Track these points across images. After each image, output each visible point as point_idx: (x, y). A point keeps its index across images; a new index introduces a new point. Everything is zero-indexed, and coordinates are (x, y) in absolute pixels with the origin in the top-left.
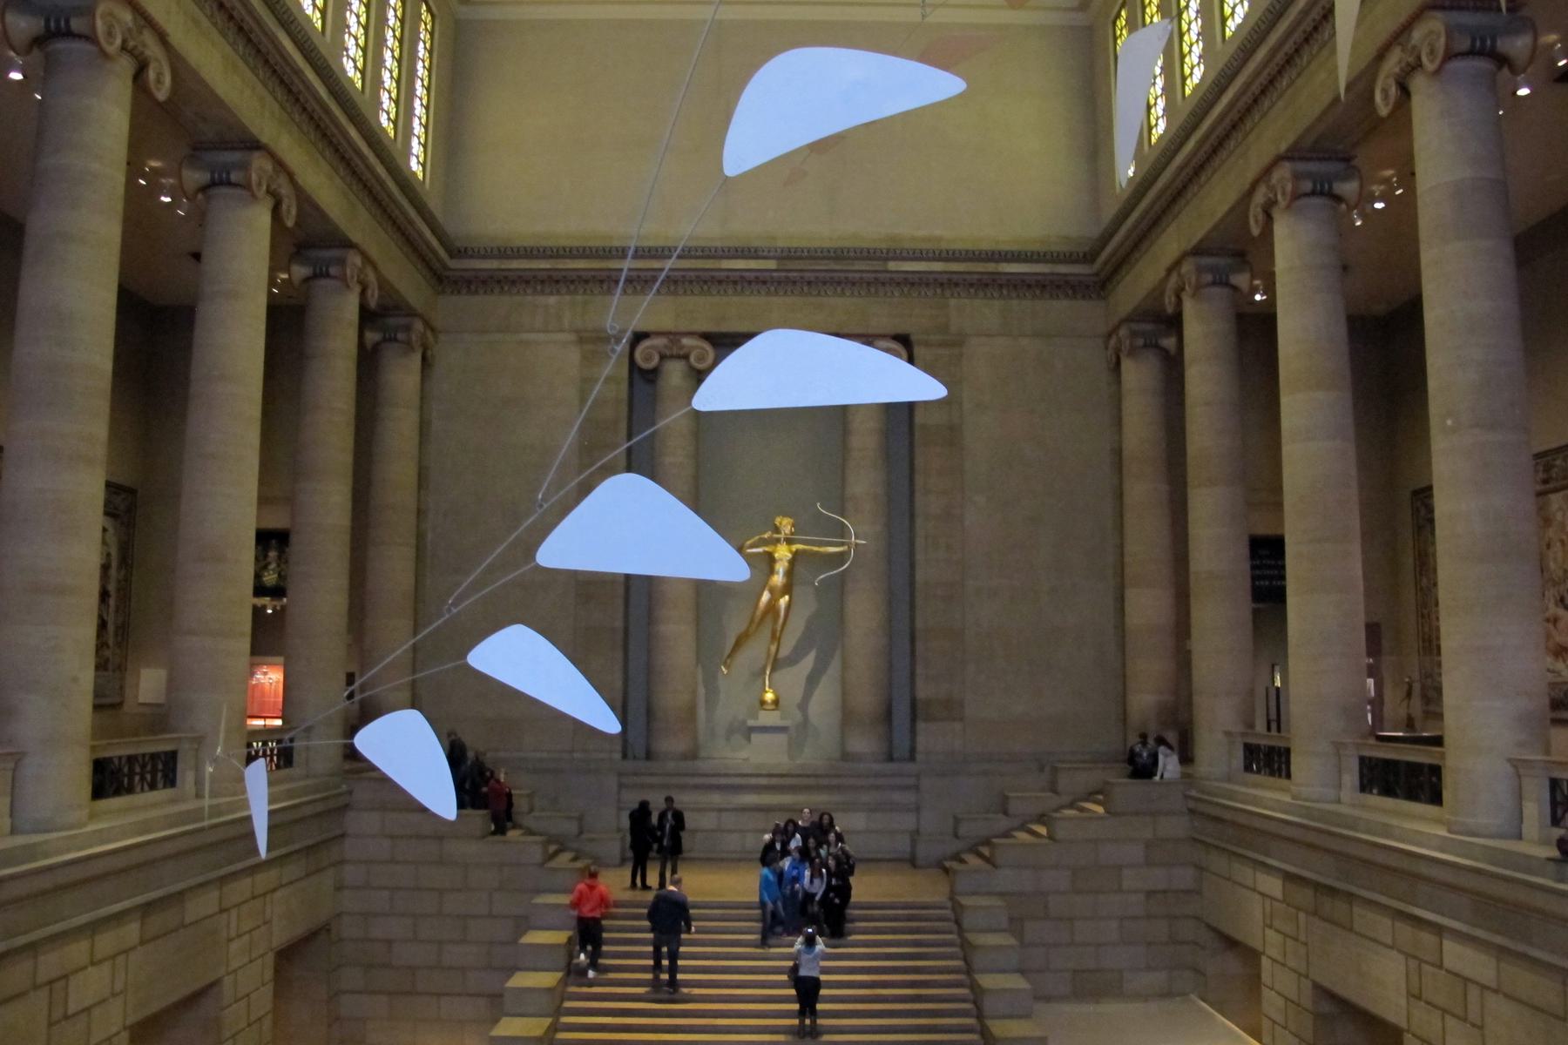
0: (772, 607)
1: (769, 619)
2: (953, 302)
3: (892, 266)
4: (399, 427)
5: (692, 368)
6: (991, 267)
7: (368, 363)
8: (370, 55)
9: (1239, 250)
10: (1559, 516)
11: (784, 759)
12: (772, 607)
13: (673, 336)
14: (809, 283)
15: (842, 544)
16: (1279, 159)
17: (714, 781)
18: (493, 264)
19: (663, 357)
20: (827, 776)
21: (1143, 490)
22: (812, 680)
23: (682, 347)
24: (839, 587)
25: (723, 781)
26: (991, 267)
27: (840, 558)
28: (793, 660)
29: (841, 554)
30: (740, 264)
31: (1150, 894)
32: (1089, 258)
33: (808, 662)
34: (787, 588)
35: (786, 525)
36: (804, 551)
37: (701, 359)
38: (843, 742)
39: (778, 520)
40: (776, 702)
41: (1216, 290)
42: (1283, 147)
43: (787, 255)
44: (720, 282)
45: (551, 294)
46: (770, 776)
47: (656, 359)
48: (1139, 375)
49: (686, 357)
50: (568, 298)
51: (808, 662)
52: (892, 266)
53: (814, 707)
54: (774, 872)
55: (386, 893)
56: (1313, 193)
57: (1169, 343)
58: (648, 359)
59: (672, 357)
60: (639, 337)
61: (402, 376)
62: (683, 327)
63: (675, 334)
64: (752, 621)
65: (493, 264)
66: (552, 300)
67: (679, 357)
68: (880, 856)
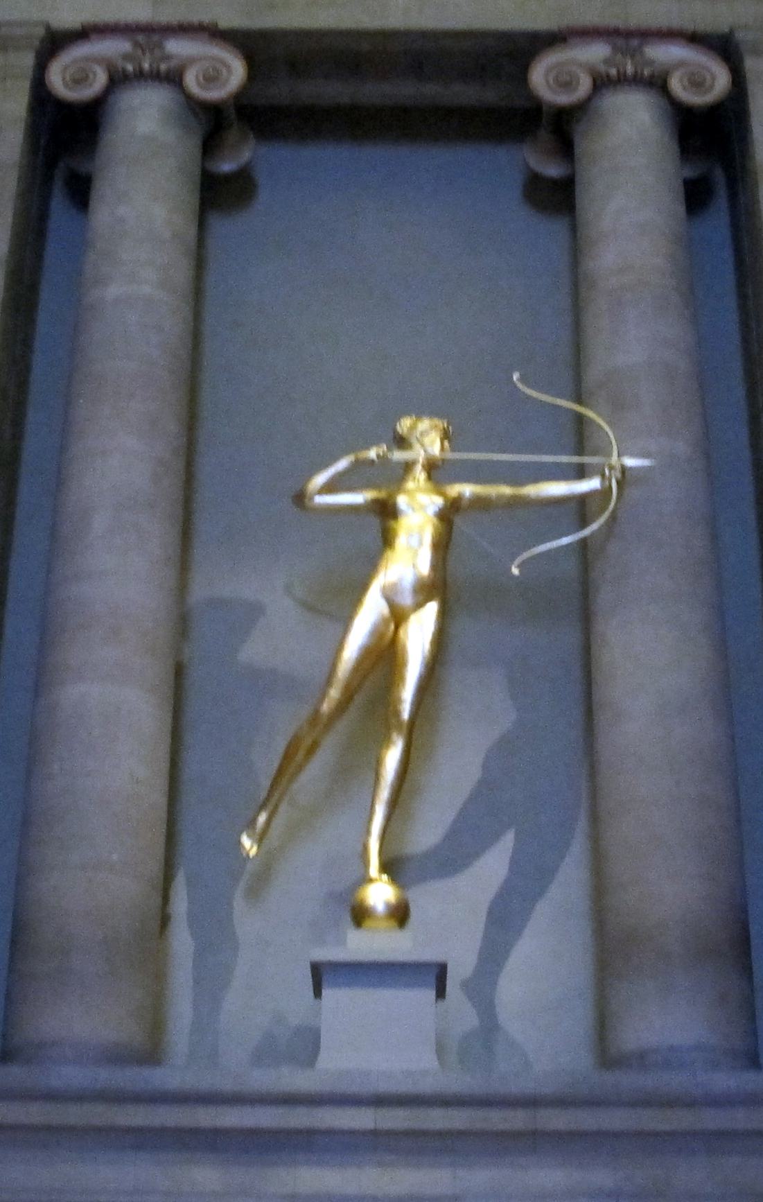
0: (384, 654)
5: (189, 99)
11: (427, 1060)
12: (384, 654)
15: (581, 473)
17: (206, 1117)
20: (561, 1102)
22: (505, 919)
23: (168, 58)
24: (576, 595)
25: (231, 1118)
27: (582, 508)
28: (452, 857)
29: (582, 500)
33: (493, 866)
35: (428, 439)
36: (480, 503)
38: (603, 1025)
39: (405, 425)
46: (380, 1101)
47: (100, 80)
51: (493, 866)
53: (516, 988)
58: (80, 80)
59: (140, 76)
62: (167, 16)
67: (637, 81)
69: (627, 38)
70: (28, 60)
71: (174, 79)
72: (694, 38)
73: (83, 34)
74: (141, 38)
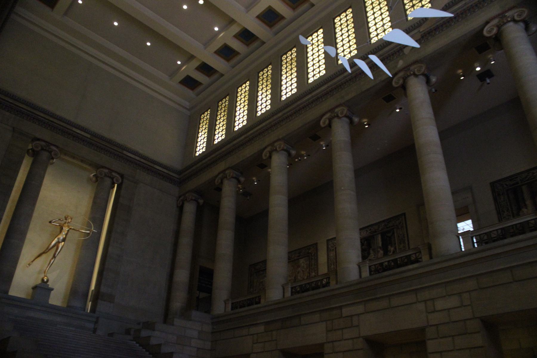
1: (55, 248)
2: (138, 170)
3: (125, 152)
9: (261, 164)
10: (302, 265)
13: (49, 144)
16: (278, 140)
19: (42, 149)
26: (152, 165)
31: (198, 349)
32: (180, 173)
34: (64, 240)
40: (436, 91)
42: (281, 137)
43: (94, 135)
47: (40, 148)
49: (50, 152)
52: (125, 152)
55: (450, 339)
56: (194, 200)
59: (45, 150)
63: (49, 143)
64: (47, 249)
66: (8, 114)
67: (110, 177)
69: (111, 171)
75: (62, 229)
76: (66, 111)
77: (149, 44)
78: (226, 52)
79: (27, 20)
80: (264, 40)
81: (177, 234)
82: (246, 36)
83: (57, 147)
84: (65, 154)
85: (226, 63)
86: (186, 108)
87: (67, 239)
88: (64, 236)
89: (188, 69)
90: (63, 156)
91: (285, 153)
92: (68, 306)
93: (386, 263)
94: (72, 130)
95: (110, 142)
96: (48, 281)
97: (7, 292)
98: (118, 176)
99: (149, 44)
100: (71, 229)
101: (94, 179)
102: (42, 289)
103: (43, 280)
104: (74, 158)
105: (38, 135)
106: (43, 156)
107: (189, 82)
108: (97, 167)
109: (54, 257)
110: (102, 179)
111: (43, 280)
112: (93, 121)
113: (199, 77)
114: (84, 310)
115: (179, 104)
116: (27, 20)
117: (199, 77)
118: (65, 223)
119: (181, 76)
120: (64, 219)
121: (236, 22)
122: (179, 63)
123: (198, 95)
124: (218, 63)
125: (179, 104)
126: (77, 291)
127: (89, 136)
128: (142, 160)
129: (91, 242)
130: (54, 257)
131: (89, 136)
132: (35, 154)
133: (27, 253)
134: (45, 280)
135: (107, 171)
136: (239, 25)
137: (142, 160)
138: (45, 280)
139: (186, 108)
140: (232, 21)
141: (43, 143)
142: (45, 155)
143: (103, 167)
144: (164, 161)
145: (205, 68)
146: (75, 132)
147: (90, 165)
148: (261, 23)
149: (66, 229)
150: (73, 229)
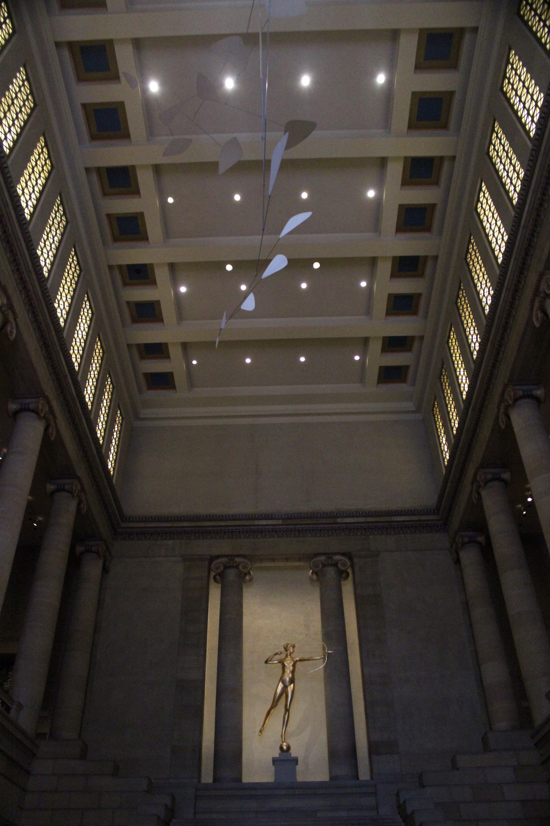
2: (371, 537)
3: (339, 520)
4: (88, 593)
6: (388, 519)
7: (74, 564)
8: (96, 397)
13: (231, 557)
14: (299, 531)
18: (142, 525)
19: (226, 567)
21: (482, 612)
26: (388, 519)
30: (264, 522)
34: (292, 681)
37: (245, 567)
41: (496, 483)
44: (254, 532)
45: (170, 539)
47: (222, 568)
48: (470, 557)
49: (237, 567)
50: (178, 541)
52: (339, 520)
54: (290, 684)
57: (481, 539)
59: (230, 567)
60: (212, 559)
61: (92, 569)
64: (273, 701)
65: (142, 525)
66: (170, 542)
68: (336, 411)
69: (329, 555)
70: (207, 563)
71: (335, 565)
72: (343, 554)
73: (218, 557)
74: (230, 558)
75: (284, 667)
76: (241, 503)
77: (302, 359)
78: (400, 305)
79: (162, 419)
80: (435, 254)
81: (467, 607)
82: (406, 266)
83: (244, 556)
84: (261, 561)
85: (414, 318)
86: (409, 412)
87: (296, 677)
88: (290, 675)
89: (377, 358)
90: (258, 565)
91: (525, 401)
92: (331, 778)
93: (159, 539)
94: (254, 525)
95: (313, 516)
96: (289, 748)
97: (239, 779)
98: (243, 560)
99: (302, 359)
100: (297, 661)
101: (315, 577)
102: (285, 760)
103: (281, 748)
104: (274, 560)
105: (215, 552)
106: (234, 576)
107: (389, 375)
108: (309, 557)
109: (287, 710)
110: (328, 572)
111: (281, 748)
112: (281, 498)
113: (395, 359)
114: (357, 778)
115: (391, 412)
116: (162, 419)
117: (395, 359)
118: (287, 656)
119: (373, 374)
120: (283, 650)
121: (378, 257)
122: (357, 358)
123: (413, 384)
124: (403, 326)
125: (391, 412)
126: (341, 750)
127: (280, 522)
128: (369, 519)
129: (337, 670)
130: (287, 710)
131: (280, 522)
132: (221, 578)
133: (252, 714)
134: (285, 748)
135: (323, 558)
136: (385, 258)
137: (369, 519)
138: (285, 748)
139: (409, 412)
140: (373, 261)
141: (224, 560)
142: (231, 574)
143: (316, 555)
144: (408, 503)
145: (393, 344)
146: (258, 525)
147: (300, 560)
148: (408, 235)
149: (289, 664)
150: (301, 660)
